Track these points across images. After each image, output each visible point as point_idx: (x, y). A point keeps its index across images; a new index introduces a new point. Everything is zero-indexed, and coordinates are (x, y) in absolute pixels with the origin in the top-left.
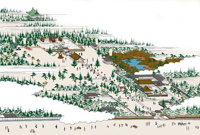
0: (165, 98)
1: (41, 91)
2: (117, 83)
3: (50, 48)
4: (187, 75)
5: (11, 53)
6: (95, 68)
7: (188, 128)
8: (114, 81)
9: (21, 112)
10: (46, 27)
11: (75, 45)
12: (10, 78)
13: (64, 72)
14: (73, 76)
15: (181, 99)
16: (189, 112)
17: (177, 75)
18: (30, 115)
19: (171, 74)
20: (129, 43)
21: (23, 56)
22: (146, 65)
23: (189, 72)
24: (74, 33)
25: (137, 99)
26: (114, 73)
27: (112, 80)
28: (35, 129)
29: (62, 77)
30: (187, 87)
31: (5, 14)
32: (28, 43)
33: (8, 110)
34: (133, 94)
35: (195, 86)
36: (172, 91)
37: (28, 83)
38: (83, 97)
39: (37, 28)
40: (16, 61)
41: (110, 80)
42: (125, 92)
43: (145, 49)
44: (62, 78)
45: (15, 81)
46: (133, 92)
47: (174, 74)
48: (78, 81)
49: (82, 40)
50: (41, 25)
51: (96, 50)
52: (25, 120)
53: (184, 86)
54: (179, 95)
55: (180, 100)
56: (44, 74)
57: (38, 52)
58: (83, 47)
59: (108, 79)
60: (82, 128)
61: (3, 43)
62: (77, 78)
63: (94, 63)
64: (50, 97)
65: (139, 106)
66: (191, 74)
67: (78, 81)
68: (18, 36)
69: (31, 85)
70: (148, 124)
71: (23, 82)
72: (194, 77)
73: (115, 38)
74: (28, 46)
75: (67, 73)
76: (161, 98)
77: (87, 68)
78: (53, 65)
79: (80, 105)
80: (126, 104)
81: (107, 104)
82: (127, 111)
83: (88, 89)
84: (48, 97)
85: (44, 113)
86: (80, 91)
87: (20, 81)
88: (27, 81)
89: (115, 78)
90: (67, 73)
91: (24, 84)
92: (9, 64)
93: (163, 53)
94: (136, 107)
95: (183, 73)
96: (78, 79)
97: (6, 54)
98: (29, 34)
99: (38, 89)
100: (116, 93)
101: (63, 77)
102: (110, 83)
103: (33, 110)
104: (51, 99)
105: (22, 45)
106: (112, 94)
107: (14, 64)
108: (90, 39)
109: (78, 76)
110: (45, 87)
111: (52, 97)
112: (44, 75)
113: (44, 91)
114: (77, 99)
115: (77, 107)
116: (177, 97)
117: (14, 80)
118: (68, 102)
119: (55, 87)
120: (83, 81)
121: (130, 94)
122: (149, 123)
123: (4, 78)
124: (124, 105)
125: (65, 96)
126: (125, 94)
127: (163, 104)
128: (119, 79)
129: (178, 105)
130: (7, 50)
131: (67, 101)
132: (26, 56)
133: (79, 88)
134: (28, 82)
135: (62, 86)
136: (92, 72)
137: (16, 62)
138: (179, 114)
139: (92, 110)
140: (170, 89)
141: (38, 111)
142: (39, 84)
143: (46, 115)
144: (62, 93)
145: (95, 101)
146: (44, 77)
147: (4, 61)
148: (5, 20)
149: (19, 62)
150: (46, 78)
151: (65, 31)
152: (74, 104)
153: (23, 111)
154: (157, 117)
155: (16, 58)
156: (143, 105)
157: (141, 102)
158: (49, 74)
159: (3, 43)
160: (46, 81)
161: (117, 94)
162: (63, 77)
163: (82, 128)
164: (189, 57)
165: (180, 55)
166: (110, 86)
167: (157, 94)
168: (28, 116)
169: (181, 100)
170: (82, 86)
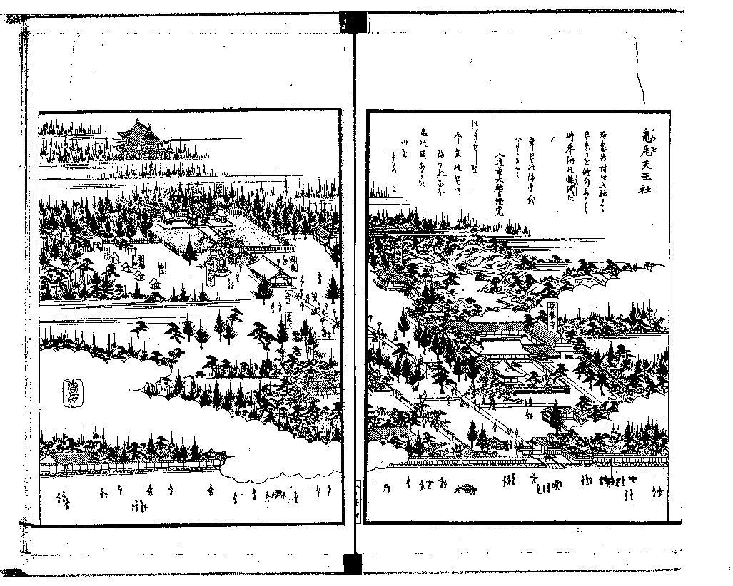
0: (562, 399)
1: (164, 379)
2: (415, 349)
3: (190, 243)
4: (629, 327)
5: (74, 262)
6: (326, 305)
7: (629, 495)
8: (409, 343)
9: (104, 446)
10: (176, 178)
11: (265, 234)
12: (69, 341)
13: (233, 318)
14: (259, 330)
15: (610, 401)
16: (631, 444)
17: (597, 324)
18: (130, 455)
19: (579, 321)
20: (454, 224)
21: (109, 269)
22: (504, 295)
23: (632, 314)
24: (261, 198)
25: (477, 403)
26: (408, 317)
27: (401, 340)
28: (147, 500)
29: (225, 333)
30: (626, 362)
31: (54, 141)
32: (124, 226)
33: (65, 440)
34: (464, 385)
35: (651, 359)
36: (584, 377)
37: (125, 355)
38: (290, 397)
39: (151, 181)
40: (87, 287)
41: (396, 339)
42: (442, 378)
43: (503, 244)
44: (226, 337)
45: (86, 348)
46: (465, 379)
47: (589, 322)
48: (274, 345)
49: (285, 217)
50: (164, 170)
51: (329, 247)
52: (99, 471)
53: (619, 360)
54: (604, 388)
55: (606, 404)
56: (172, 325)
57: (162, 261)
58: (290, 238)
59: (391, 337)
60: (290, 495)
61: (49, 231)
62: (271, 336)
63: (323, 289)
64: (191, 396)
65: (483, 423)
66: (640, 322)
67: (274, 345)
68: (94, 206)
69: (133, 359)
70: (509, 480)
71: (109, 352)
72: (649, 331)
73: (413, 208)
74: (125, 236)
75: (240, 320)
76: (549, 399)
77: (303, 305)
78: (198, 295)
79: (283, 421)
80: (442, 418)
81: (387, 417)
82: (444, 440)
83: (304, 369)
84: (184, 397)
85: (172, 449)
86: (282, 377)
87: (101, 350)
88: (122, 348)
89: (410, 334)
90: (240, 320)
91: (113, 357)
92: (69, 296)
93: (555, 257)
94: (473, 425)
95: (614, 319)
96: (274, 339)
97: (57, 263)
98: (128, 199)
99: (154, 372)
100: (412, 383)
101: (230, 335)
102: (396, 348)
103: (141, 438)
104: (194, 405)
105: (106, 236)
106: (401, 384)
107: (84, 294)
108: (310, 214)
109: (273, 330)
110: (174, 365)
111: (198, 395)
112: (173, 328)
113: (173, 378)
114: (271, 402)
115: (272, 427)
116: (598, 396)
117: (83, 345)
118: (245, 412)
119: (205, 366)
120: (289, 346)
121: (453, 385)
122: (513, 478)
123: (52, 340)
124: (437, 419)
125: (235, 392)
126: (441, 385)
127: (555, 416)
128: (422, 338)
129: (601, 422)
130: (62, 249)
131: (241, 410)
132: (119, 269)
133: (279, 367)
134: (126, 352)
135: (226, 363)
136: (318, 318)
137: (89, 288)
138: (602, 448)
139: (318, 437)
140: (577, 369)
141: (156, 440)
142: (157, 357)
143: (180, 454)
144: (225, 385)
145: (326, 408)
146: (173, 333)
147: (54, 287)
148: (56, 157)
149: (96, 289)
150: (180, 339)
151: (235, 189)
152: (262, 420)
153: (112, 443)
154: (538, 459)
155: (89, 275)
156: (494, 421)
157: (487, 410)
158: (188, 324)
159: (49, 231)
160: (178, 346)
161: (415, 385)
162: (230, 335)
163: (290, 495)
164: (636, 268)
165: (607, 264)
166: (393, 360)
167: (538, 385)
168: (124, 458)
169: (609, 405)
170: (288, 361)
